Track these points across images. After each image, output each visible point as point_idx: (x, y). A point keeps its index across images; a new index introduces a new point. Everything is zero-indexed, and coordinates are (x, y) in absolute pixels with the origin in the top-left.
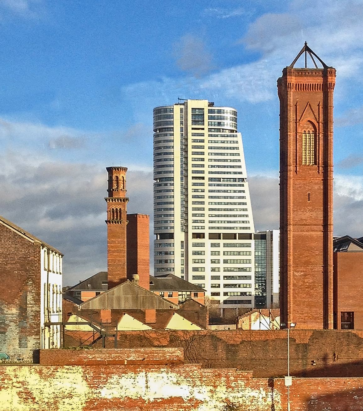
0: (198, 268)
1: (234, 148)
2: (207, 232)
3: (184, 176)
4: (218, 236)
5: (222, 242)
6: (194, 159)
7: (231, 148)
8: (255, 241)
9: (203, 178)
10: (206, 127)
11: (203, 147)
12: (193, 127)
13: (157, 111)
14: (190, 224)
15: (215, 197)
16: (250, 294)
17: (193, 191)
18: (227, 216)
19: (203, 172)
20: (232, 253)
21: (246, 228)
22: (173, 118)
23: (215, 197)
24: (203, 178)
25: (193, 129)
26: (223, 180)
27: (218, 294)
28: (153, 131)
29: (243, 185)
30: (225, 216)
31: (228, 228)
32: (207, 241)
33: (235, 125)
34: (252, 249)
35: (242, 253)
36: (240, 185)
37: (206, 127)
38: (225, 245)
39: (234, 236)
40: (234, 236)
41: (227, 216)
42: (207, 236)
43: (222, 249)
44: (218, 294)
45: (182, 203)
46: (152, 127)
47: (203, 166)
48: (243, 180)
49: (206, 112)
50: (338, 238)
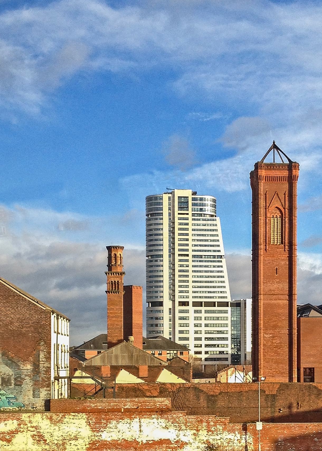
0: (183, 331)
1: (213, 230)
2: (191, 300)
3: (172, 253)
4: (200, 304)
5: (203, 309)
7: (211, 230)
8: (231, 308)
9: (188, 255)
10: (190, 212)
11: (187, 229)
12: (179, 213)
13: (149, 199)
14: (177, 294)
15: (198, 271)
16: (227, 353)
17: (179, 266)
19: (187, 250)
20: (212, 318)
21: (224, 297)
22: (162, 205)
23: (198, 271)
24: (187, 255)
25: (179, 214)
27: (200, 353)
28: (146, 215)
29: (221, 261)
30: (206, 287)
31: (208, 297)
32: (191, 308)
34: (229, 315)
35: (221, 318)
36: (219, 261)
37: (190, 212)
38: (206, 312)
39: (213, 304)
40: (213, 304)
42: (191, 304)
43: (203, 315)
44: (200, 353)
45: (170, 276)
46: (145, 213)
47: (187, 245)
48: (221, 257)
49: (190, 199)
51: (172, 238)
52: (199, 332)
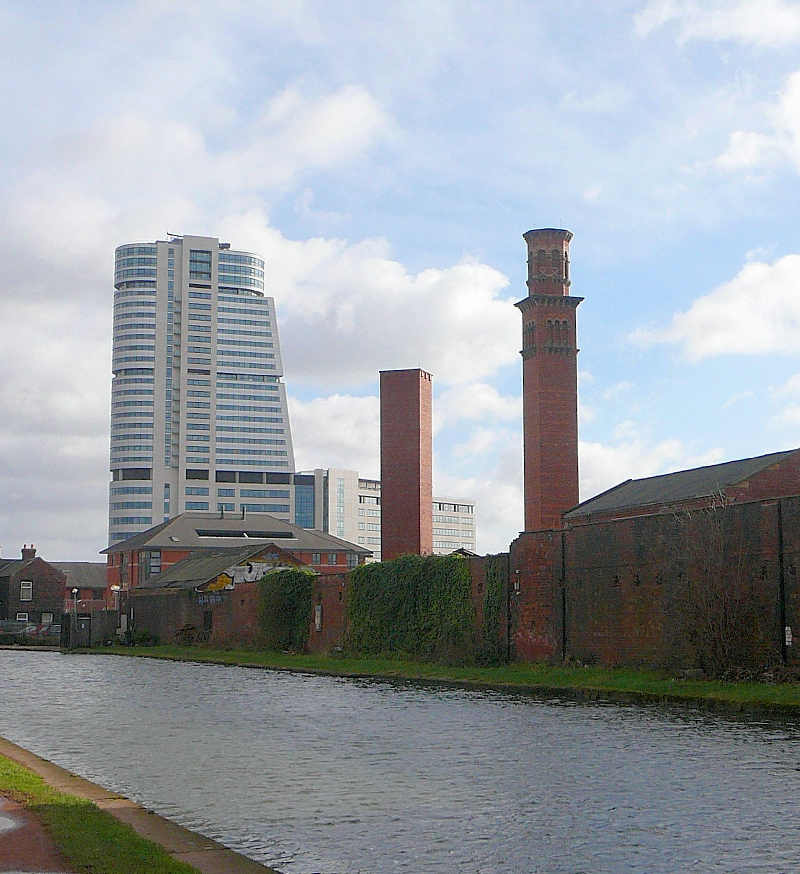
2: (213, 469)
5: (237, 487)
6: (206, 405)
7: (256, 344)
9: (207, 373)
13: (210, 286)
25: (191, 285)
26: (242, 292)
33: (260, 272)
34: (291, 501)
37: (215, 283)
38: (244, 493)
39: (247, 477)
42: (212, 476)
49: (215, 257)
50: (268, 546)
51: (176, 312)
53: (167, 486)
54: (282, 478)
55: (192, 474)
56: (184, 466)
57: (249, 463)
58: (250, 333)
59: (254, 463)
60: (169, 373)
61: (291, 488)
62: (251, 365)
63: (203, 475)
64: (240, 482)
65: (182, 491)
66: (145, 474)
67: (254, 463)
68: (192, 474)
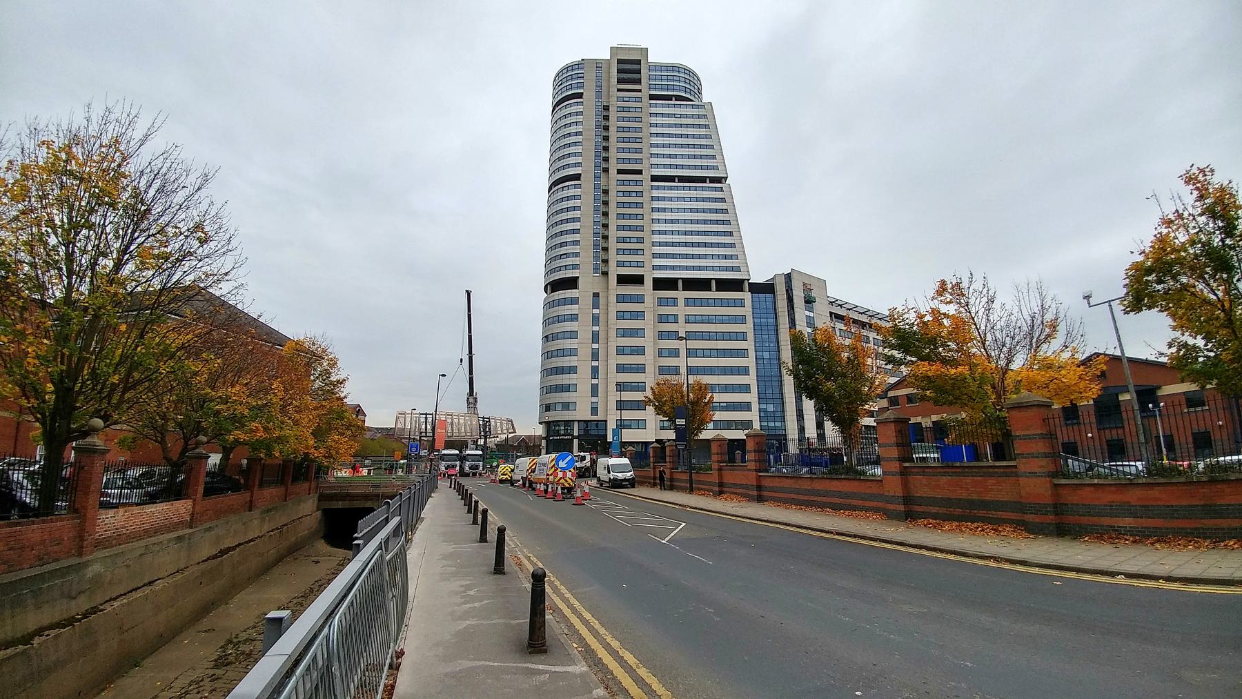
4: (669, 284)
5: (681, 295)
14: (613, 257)
18: (701, 157)
25: (619, 90)
34: (747, 311)
38: (688, 303)
39: (691, 284)
40: (703, 285)
41: (701, 157)
42: (648, 283)
43: (681, 310)
52: (665, 353)
53: (596, 295)
54: (736, 285)
55: (623, 280)
56: (614, 271)
57: (693, 268)
58: (693, 256)
59: (700, 268)
60: (597, 177)
61: (747, 295)
62: (689, 156)
63: (638, 280)
64: (683, 290)
65: (613, 299)
66: (572, 283)
67: (700, 268)
68: (623, 280)
